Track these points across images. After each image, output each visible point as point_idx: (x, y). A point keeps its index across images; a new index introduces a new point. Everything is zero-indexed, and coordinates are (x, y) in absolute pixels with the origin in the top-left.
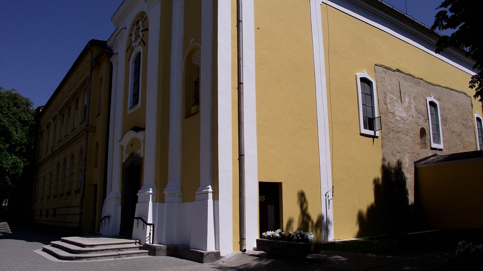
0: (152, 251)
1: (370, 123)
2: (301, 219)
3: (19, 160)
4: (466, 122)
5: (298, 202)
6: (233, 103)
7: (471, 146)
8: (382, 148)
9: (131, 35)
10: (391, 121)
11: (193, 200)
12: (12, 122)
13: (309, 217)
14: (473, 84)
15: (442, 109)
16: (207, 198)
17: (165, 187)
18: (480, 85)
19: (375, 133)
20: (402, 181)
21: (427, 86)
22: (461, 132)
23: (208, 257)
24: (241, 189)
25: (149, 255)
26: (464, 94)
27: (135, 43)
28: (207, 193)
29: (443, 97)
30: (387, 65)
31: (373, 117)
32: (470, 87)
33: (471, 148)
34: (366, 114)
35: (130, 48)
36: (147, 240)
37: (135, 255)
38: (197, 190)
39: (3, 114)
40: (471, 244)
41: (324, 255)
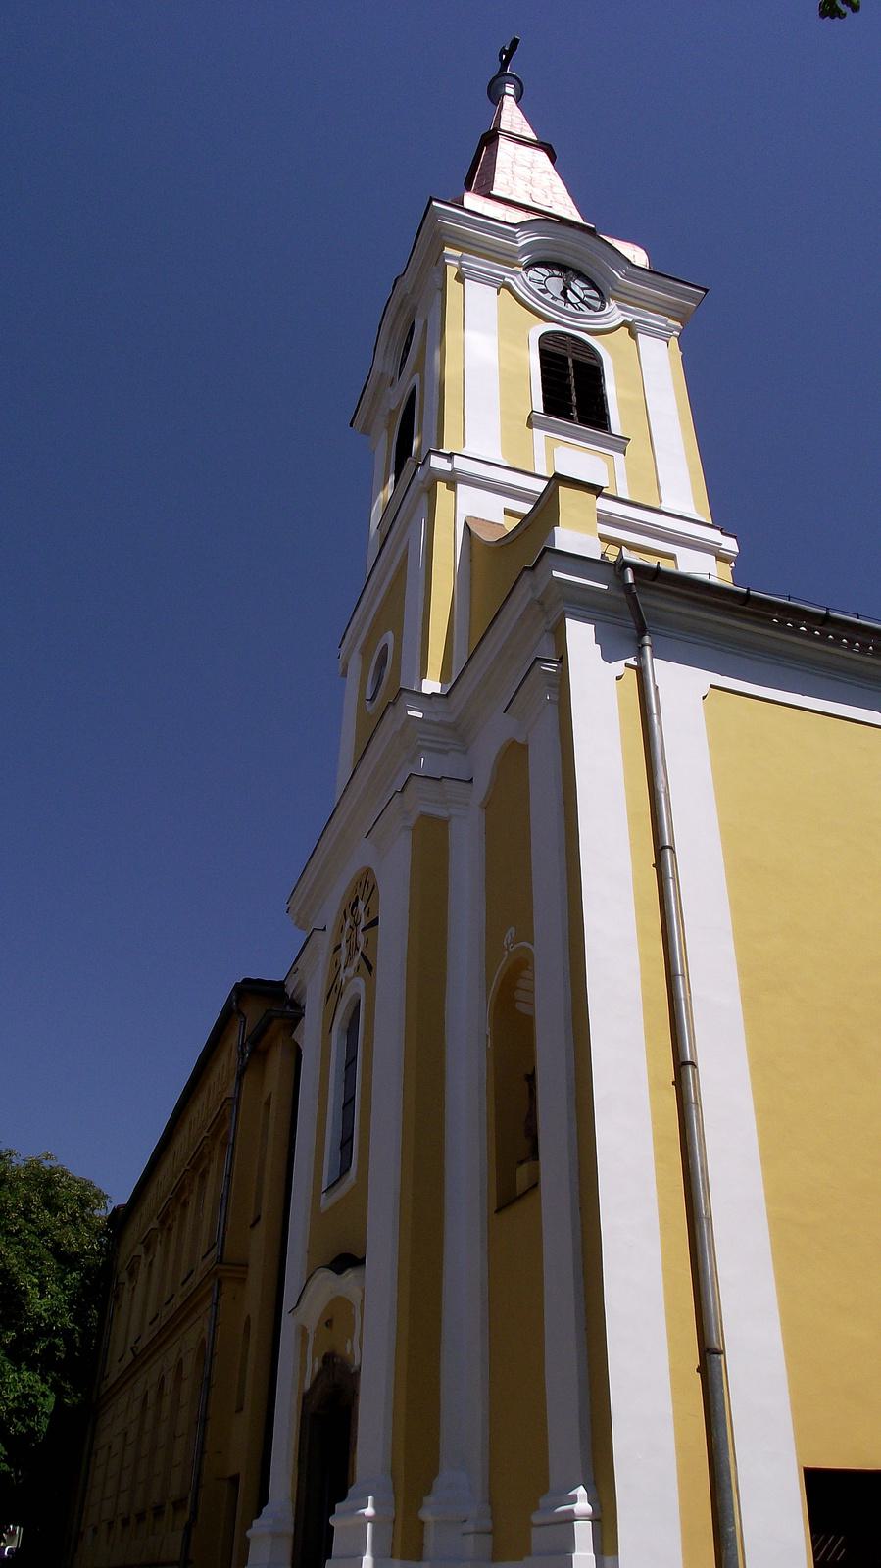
3: (42, 1387)
6: (658, 1139)
11: (523, 1550)
12: (33, 1257)
28: (570, 1519)
38: (537, 1508)
39: (9, 1233)
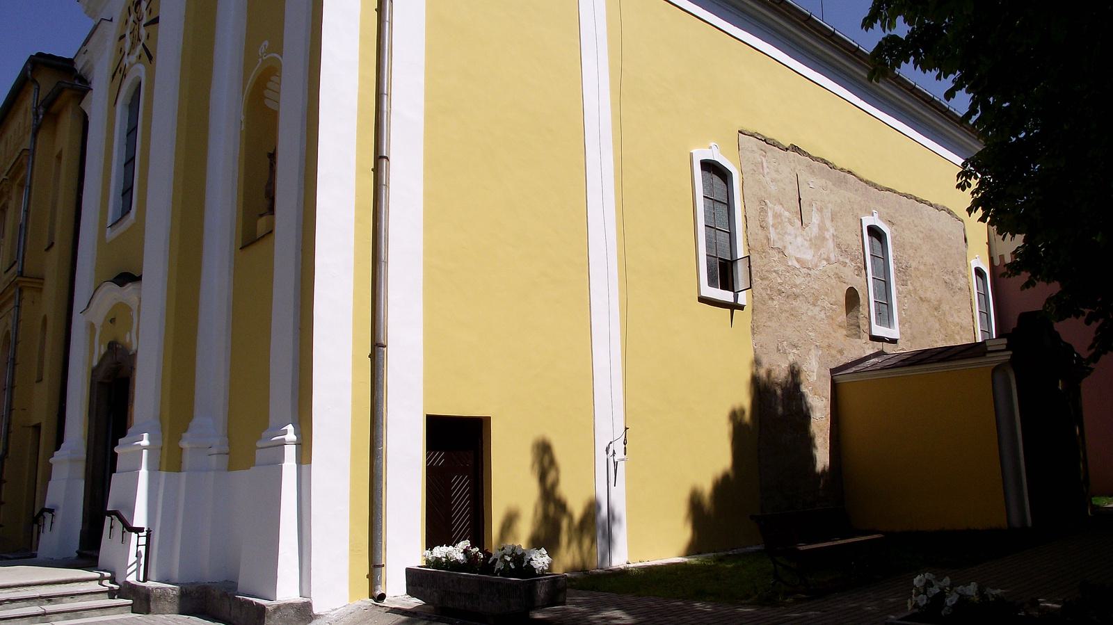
0: (141, 601)
1: (724, 273)
2: (540, 510)
4: (952, 278)
5: (533, 465)
6: (358, 207)
7: (962, 333)
8: (753, 334)
9: (123, 37)
10: (776, 269)
13: (562, 507)
14: (966, 181)
15: (899, 246)
16: (280, 459)
17: (186, 431)
18: (981, 183)
19: (736, 297)
20: (802, 416)
21: (864, 190)
22: (940, 301)
23: (277, 616)
24: (376, 436)
25: (132, 612)
26: (949, 213)
27: (130, 56)
28: (282, 444)
29: (901, 218)
30: (769, 134)
31: (731, 257)
32: (958, 186)
33: (961, 338)
34: (714, 250)
36: (129, 571)
37: (93, 612)
38: (260, 438)
40: (947, 581)
41: (580, 609)
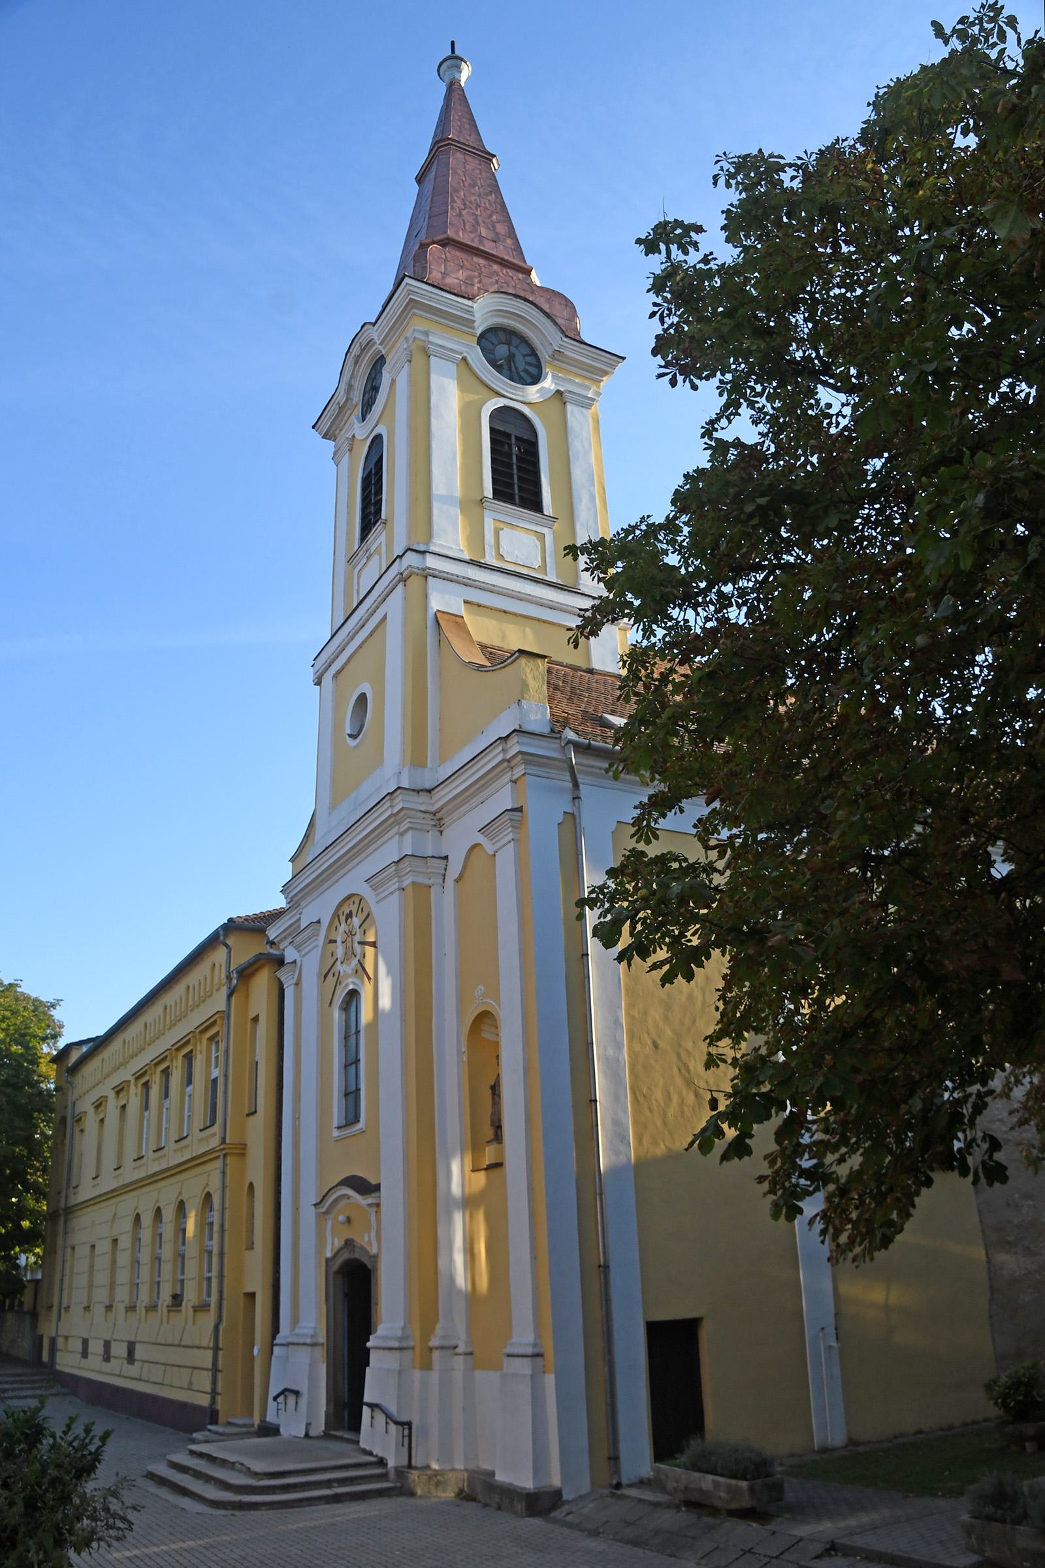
10: (1000, 1117)
27: (344, 965)
35: (331, 972)
